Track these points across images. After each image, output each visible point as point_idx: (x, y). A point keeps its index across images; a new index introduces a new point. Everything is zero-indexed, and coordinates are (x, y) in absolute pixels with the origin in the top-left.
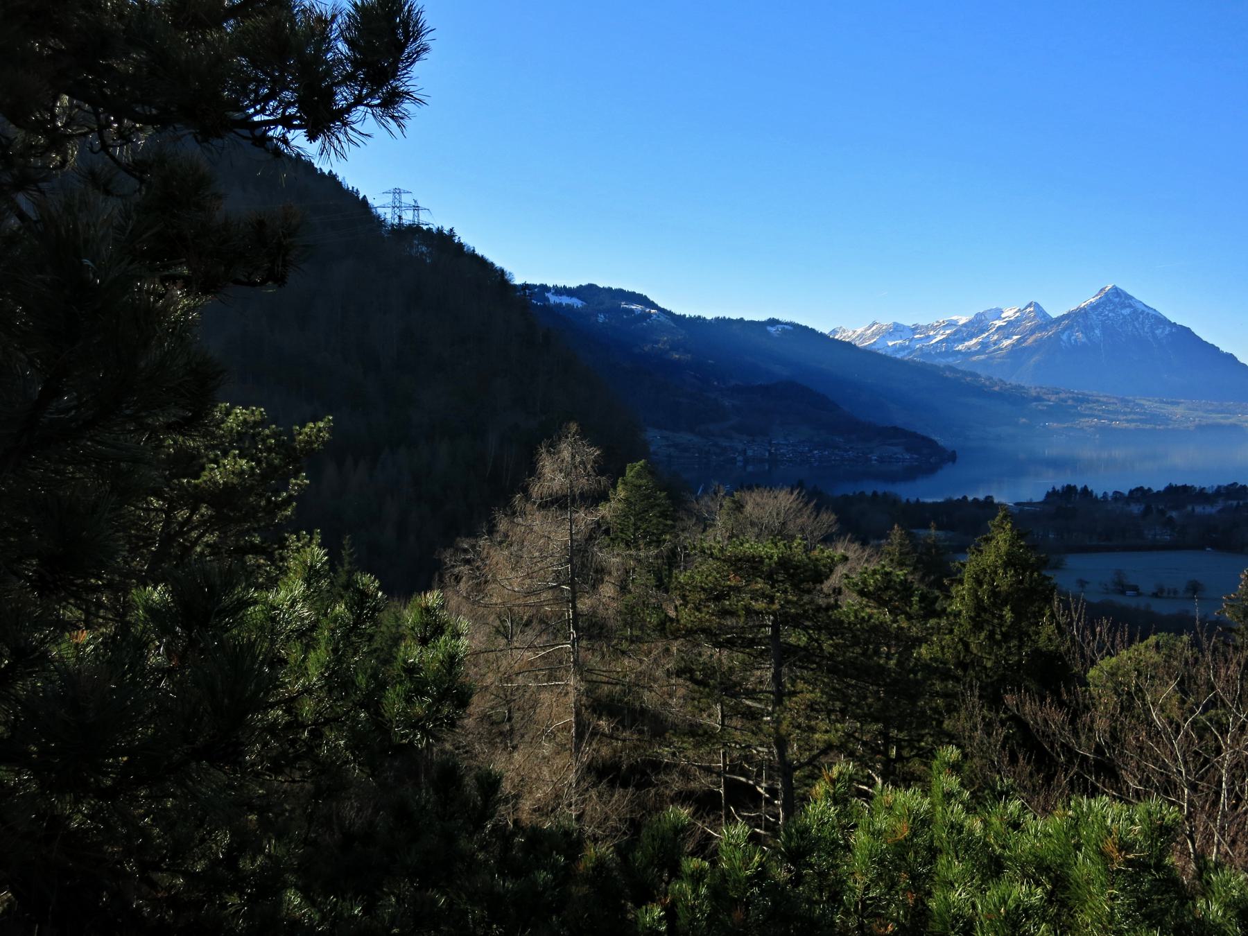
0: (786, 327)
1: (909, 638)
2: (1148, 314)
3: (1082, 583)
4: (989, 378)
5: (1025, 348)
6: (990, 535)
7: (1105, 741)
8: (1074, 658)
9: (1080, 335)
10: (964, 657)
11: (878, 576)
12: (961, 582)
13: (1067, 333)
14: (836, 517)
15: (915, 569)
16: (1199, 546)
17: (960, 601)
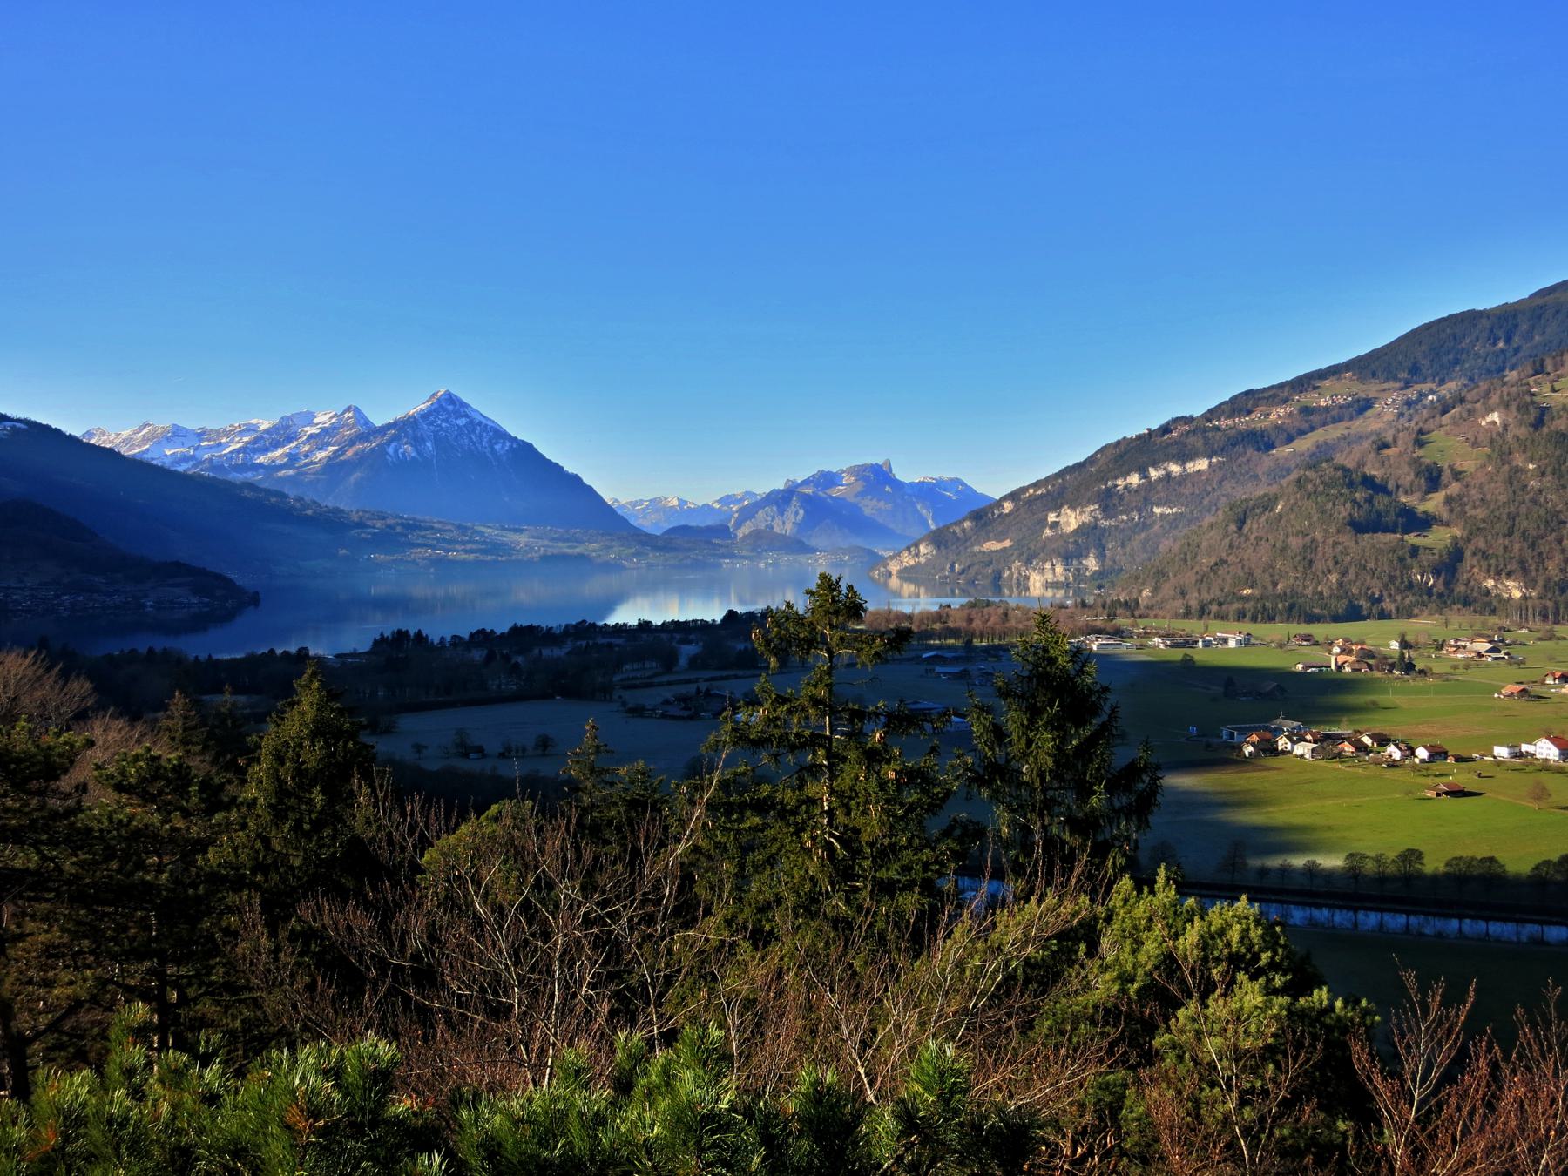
0: (18, 425)
1: (187, 840)
2: (486, 425)
3: (418, 748)
4: (299, 499)
5: (345, 461)
6: (295, 698)
7: (421, 943)
8: (380, 848)
9: (409, 448)
10: (264, 857)
11: (142, 763)
12: (259, 761)
13: (393, 445)
14: (91, 686)
15: (205, 748)
16: (545, 696)
17: (256, 789)
